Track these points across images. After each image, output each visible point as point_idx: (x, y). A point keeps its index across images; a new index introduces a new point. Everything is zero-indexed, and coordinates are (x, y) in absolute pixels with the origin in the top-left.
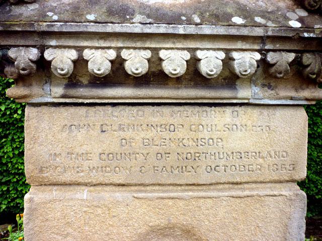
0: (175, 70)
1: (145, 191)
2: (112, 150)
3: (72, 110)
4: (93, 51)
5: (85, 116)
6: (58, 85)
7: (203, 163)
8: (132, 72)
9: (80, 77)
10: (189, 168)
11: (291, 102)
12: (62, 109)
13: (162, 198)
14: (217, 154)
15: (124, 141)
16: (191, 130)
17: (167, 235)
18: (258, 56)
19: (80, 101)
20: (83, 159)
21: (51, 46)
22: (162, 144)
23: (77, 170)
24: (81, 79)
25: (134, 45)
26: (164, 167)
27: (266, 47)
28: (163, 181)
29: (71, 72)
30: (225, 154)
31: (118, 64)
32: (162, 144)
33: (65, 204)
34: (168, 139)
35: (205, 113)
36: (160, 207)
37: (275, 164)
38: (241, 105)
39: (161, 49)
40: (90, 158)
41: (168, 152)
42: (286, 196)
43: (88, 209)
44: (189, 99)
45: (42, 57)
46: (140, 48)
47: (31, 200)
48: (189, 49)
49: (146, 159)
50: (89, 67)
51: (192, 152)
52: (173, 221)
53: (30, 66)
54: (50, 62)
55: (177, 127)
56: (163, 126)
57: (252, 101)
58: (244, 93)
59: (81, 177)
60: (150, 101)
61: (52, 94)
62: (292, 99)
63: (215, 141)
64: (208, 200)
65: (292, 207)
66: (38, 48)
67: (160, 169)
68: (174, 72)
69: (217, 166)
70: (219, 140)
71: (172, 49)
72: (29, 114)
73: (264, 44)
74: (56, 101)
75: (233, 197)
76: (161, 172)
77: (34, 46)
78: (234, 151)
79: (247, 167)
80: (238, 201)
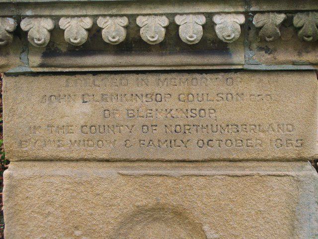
0: (153, 37)
1: (132, 168)
2: (94, 123)
3: (52, 79)
4: (69, 20)
5: (64, 85)
6: (35, 54)
7: (194, 136)
8: (109, 40)
9: (58, 45)
10: (179, 142)
11: (291, 67)
12: (41, 79)
13: (150, 175)
14: (210, 127)
15: (106, 112)
16: (180, 100)
17: (157, 218)
18: (241, 19)
19: (59, 70)
20: (64, 133)
21: (27, 16)
22: (149, 115)
23: (58, 144)
24: (59, 47)
25: (110, 13)
26: (150, 140)
27: (252, 9)
28: (151, 157)
29: (47, 42)
30: (219, 127)
31: (95, 32)
32: (149, 115)
33: (46, 180)
34: (154, 109)
35: (194, 81)
36: (146, 185)
37: (279, 139)
38: (236, 71)
39: (138, 15)
40: (72, 131)
41: (154, 124)
42: (293, 177)
43: (70, 186)
44: (174, 66)
45: (18, 27)
46: (116, 16)
47: (10, 177)
48: (168, 14)
49: (131, 132)
50: (65, 37)
51: (181, 124)
52: (162, 201)
53: (7, 36)
54: (26, 33)
55: (165, 97)
56: (149, 96)
57: (246, 67)
58: (239, 58)
59: (63, 153)
60: (133, 69)
61: (30, 63)
62: (294, 63)
63: (207, 111)
64: (200, 178)
65: (300, 189)
66: (14, 18)
67: (146, 143)
68: (151, 40)
69: (210, 140)
70: (212, 111)
71: (150, 15)
72: (6, 85)
73: (250, 6)
74: (34, 70)
75: (229, 176)
76: (148, 146)
77: (11, 17)
78: (230, 123)
79: (245, 141)
80: (235, 180)
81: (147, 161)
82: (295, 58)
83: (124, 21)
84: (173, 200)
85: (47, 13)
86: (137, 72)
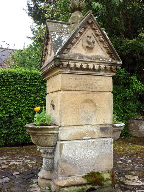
11: (109, 75)
12: (68, 75)
52: (89, 98)
57: (103, 75)
59: (72, 89)
62: (110, 75)
81: (86, 91)
82: (110, 74)
83: (86, 65)
84: (91, 98)
85: (74, 62)
86: (78, 74)
